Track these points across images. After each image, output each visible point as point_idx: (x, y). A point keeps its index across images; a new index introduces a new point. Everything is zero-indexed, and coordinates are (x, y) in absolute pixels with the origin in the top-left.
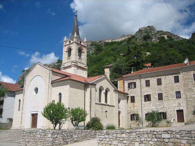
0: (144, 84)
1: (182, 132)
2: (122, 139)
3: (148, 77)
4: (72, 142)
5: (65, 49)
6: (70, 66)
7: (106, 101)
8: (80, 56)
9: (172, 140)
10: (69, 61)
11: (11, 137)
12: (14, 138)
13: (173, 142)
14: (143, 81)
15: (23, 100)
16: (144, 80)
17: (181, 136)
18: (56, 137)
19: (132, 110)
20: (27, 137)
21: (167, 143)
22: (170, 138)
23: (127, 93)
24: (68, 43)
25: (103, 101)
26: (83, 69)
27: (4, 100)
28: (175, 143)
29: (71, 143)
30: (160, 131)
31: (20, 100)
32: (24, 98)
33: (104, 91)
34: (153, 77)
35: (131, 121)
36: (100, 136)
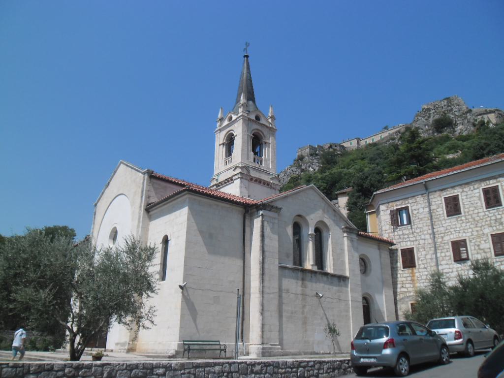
0: (442, 210)
3: (453, 187)
5: (220, 138)
10: (229, 166)
14: (438, 201)
16: (439, 199)
19: (410, 292)
23: (389, 240)
24: (226, 122)
25: (309, 263)
34: (467, 184)
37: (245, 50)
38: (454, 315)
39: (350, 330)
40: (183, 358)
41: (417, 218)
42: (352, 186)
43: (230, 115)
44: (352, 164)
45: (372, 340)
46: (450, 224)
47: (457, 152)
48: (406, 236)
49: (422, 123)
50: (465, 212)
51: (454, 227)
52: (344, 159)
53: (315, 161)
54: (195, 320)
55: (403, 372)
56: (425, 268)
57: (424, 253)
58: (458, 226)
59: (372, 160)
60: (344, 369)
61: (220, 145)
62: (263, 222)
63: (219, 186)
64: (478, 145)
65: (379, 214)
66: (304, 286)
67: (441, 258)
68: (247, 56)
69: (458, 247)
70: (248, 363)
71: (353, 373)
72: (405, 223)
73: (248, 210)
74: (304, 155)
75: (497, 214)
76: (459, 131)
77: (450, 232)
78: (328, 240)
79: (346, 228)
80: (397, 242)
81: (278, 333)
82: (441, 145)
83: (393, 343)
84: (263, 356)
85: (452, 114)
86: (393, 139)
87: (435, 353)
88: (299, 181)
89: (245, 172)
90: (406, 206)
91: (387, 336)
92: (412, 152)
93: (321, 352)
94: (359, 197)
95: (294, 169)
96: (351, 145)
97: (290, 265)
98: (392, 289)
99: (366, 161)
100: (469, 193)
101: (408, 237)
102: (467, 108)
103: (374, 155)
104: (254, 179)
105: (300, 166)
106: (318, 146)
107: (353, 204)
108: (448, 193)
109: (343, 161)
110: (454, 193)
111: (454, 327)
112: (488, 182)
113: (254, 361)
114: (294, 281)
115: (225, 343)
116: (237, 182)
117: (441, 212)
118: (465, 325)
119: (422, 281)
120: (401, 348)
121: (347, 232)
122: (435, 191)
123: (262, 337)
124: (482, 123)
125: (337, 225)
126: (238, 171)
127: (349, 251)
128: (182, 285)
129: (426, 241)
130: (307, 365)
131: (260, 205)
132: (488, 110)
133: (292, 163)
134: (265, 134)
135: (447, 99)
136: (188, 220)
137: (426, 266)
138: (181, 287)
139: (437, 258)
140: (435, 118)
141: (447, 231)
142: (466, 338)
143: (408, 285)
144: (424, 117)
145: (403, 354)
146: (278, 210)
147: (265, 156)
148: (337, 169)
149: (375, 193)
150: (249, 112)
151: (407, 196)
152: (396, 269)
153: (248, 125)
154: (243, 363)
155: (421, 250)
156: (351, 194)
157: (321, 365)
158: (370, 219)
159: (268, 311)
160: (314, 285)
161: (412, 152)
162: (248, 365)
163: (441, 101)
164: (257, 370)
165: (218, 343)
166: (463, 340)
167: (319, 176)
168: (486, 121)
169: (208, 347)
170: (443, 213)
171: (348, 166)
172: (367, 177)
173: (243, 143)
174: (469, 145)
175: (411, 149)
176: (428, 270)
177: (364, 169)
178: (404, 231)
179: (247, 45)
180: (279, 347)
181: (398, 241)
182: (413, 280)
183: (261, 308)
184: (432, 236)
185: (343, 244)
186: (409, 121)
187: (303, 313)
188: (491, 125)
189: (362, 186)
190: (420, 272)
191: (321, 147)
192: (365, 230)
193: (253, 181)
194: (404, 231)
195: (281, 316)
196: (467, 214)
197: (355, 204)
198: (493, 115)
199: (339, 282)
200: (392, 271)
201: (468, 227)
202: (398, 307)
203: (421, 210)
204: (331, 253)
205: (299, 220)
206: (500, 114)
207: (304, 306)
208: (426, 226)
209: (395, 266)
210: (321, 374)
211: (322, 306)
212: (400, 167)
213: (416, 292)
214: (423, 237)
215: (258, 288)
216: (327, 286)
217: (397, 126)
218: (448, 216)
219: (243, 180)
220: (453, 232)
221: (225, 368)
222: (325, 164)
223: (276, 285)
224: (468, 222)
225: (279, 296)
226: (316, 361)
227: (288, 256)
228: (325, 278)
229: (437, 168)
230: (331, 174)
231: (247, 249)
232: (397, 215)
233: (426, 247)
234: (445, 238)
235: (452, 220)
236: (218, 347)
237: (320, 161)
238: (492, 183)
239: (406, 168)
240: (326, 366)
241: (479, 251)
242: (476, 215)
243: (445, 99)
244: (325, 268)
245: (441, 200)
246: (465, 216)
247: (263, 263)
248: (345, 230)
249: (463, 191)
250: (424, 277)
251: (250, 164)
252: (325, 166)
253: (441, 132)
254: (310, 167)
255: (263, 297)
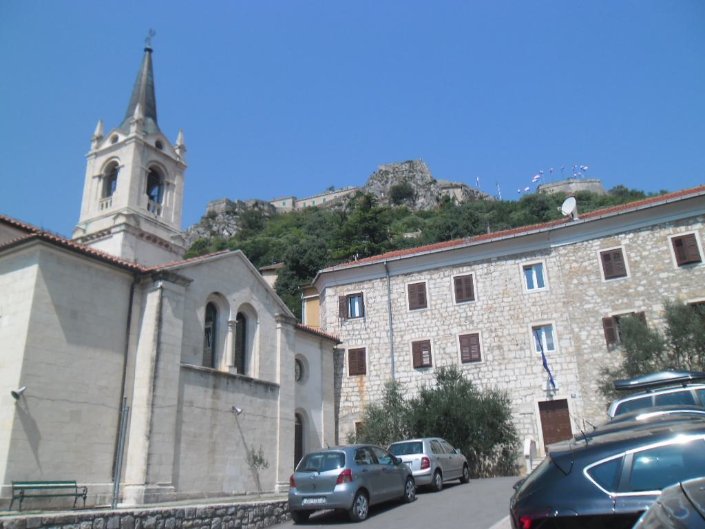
0: (403, 300)
3: (419, 272)
5: (95, 167)
14: (401, 288)
16: (402, 285)
19: (356, 407)
24: (107, 144)
25: (226, 364)
34: (437, 269)
37: (147, 40)
38: (419, 436)
39: (275, 460)
40: (10, 510)
41: (372, 309)
42: (285, 261)
43: (115, 133)
44: (284, 233)
45: (321, 473)
46: (412, 320)
47: (417, 231)
48: (357, 333)
49: (378, 189)
50: (431, 305)
51: (417, 323)
52: (273, 223)
53: (233, 222)
54: (35, 448)
55: (361, 514)
56: (377, 375)
57: (377, 356)
58: (422, 322)
59: (311, 229)
60: (277, 516)
61: (94, 177)
62: (161, 299)
63: (87, 240)
64: (445, 223)
65: (324, 300)
66: (215, 396)
67: (398, 364)
68: (150, 51)
69: (421, 351)
70: (135, 514)
71: (288, 520)
72: (357, 314)
73: (139, 279)
74: (217, 212)
75: (468, 310)
76: (420, 205)
77: (412, 329)
78: (254, 331)
79: (282, 316)
80: (344, 340)
81: (171, 467)
82: (399, 219)
83: (350, 474)
84: (146, 502)
85: (414, 183)
86: (340, 205)
87: (401, 488)
88: (208, 248)
89: (132, 223)
90: (359, 292)
91: (342, 466)
92: (366, 224)
93: (234, 492)
94: (292, 277)
95: (201, 230)
96: (284, 206)
97: (198, 365)
98: (334, 404)
99: (303, 230)
100: (439, 280)
101: (359, 334)
102: (431, 177)
103: (314, 223)
104: (146, 235)
105: (210, 227)
106: (238, 201)
107: (283, 286)
108: (413, 278)
109: (272, 226)
110: (420, 279)
111: (422, 452)
112: (461, 269)
113: (145, 510)
114: (202, 389)
115: (84, 485)
116: (118, 238)
117: (403, 304)
118: (434, 450)
119: (372, 393)
120: (358, 483)
121: (282, 322)
122: (398, 276)
123: (147, 473)
124: (447, 199)
125: (269, 311)
126: (121, 220)
127: (283, 349)
128: (17, 391)
129: (382, 339)
130: (226, 512)
131: (160, 273)
132: (454, 184)
133: (198, 221)
134: (168, 170)
135: (410, 162)
136: (37, 286)
137: (379, 373)
138: (15, 395)
139: (393, 363)
140: (393, 184)
141: (407, 328)
142: (434, 465)
143: (354, 398)
144: (380, 181)
145: (362, 491)
146: (186, 282)
147: (166, 201)
148: (263, 236)
149: (321, 271)
150: (147, 133)
151: (361, 279)
152: (340, 376)
153: (142, 153)
154: (127, 514)
155: (374, 351)
156: (281, 271)
157: (245, 512)
158: (306, 308)
159: (160, 433)
160: (230, 395)
161: (366, 224)
162: (136, 517)
163: (402, 164)
164: (150, 526)
165: (74, 485)
166: (432, 469)
167: (237, 243)
168: (451, 197)
169: (55, 492)
170: (405, 305)
171: (278, 234)
172: (306, 251)
173: (133, 179)
174: (431, 223)
175: (363, 220)
176: (382, 378)
177: (299, 241)
178: (355, 326)
179: (152, 33)
180: (172, 487)
181: (346, 339)
182: (361, 392)
183: (149, 429)
184: (389, 334)
185: (274, 339)
186: (361, 185)
187: (211, 436)
188: (457, 203)
189: (298, 262)
190: (371, 381)
191: (242, 204)
192: (301, 322)
193: (144, 238)
194: (355, 326)
195: (178, 441)
196: (433, 308)
197: (286, 285)
198: (460, 190)
199: (266, 391)
200: (335, 378)
201: (433, 325)
202: (340, 427)
203: (379, 299)
204: (257, 349)
205: (215, 300)
206: (466, 191)
207: (213, 427)
208: (383, 320)
209: (339, 373)
210: (246, 524)
211: (239, 427)
212: (349, 242)
213: (365, 408)
214: (378, 335)
215: (145, 399)
216: (248, 398)
217: (345, 188)
218: (411, 309)
219: (129, 235)
220: (416, 331)
221: (97, 524)
222: (246, 228)
223: (173, 393)
224: (434, 319)
225: (178, 411)
226: (239, 505)
227: (195, 351)
228: (246, 386)
229: (393, 248)
230: (254, 242)
231: (132, 338)
232: (347, 301)
233: (380, 348)
234: (405, 338)
235: (416, 315)
236: (73, 491)
237: (240, 223)
238: (465, 271)
239: (357, 244)
240: (252, 512)
241: (444, 355)
242: (445, 310)
243: (406, 162)
244: (248, 371)
245: (404, 288)
246: (432, 310)
247: (157, 360)
248: (280, 319)
249: (431, 279)
250: (375, 388)
251: (142, 212)
252: (246, 230)
253: (399, 204)
254: (225, 231)
255: (152, 412)
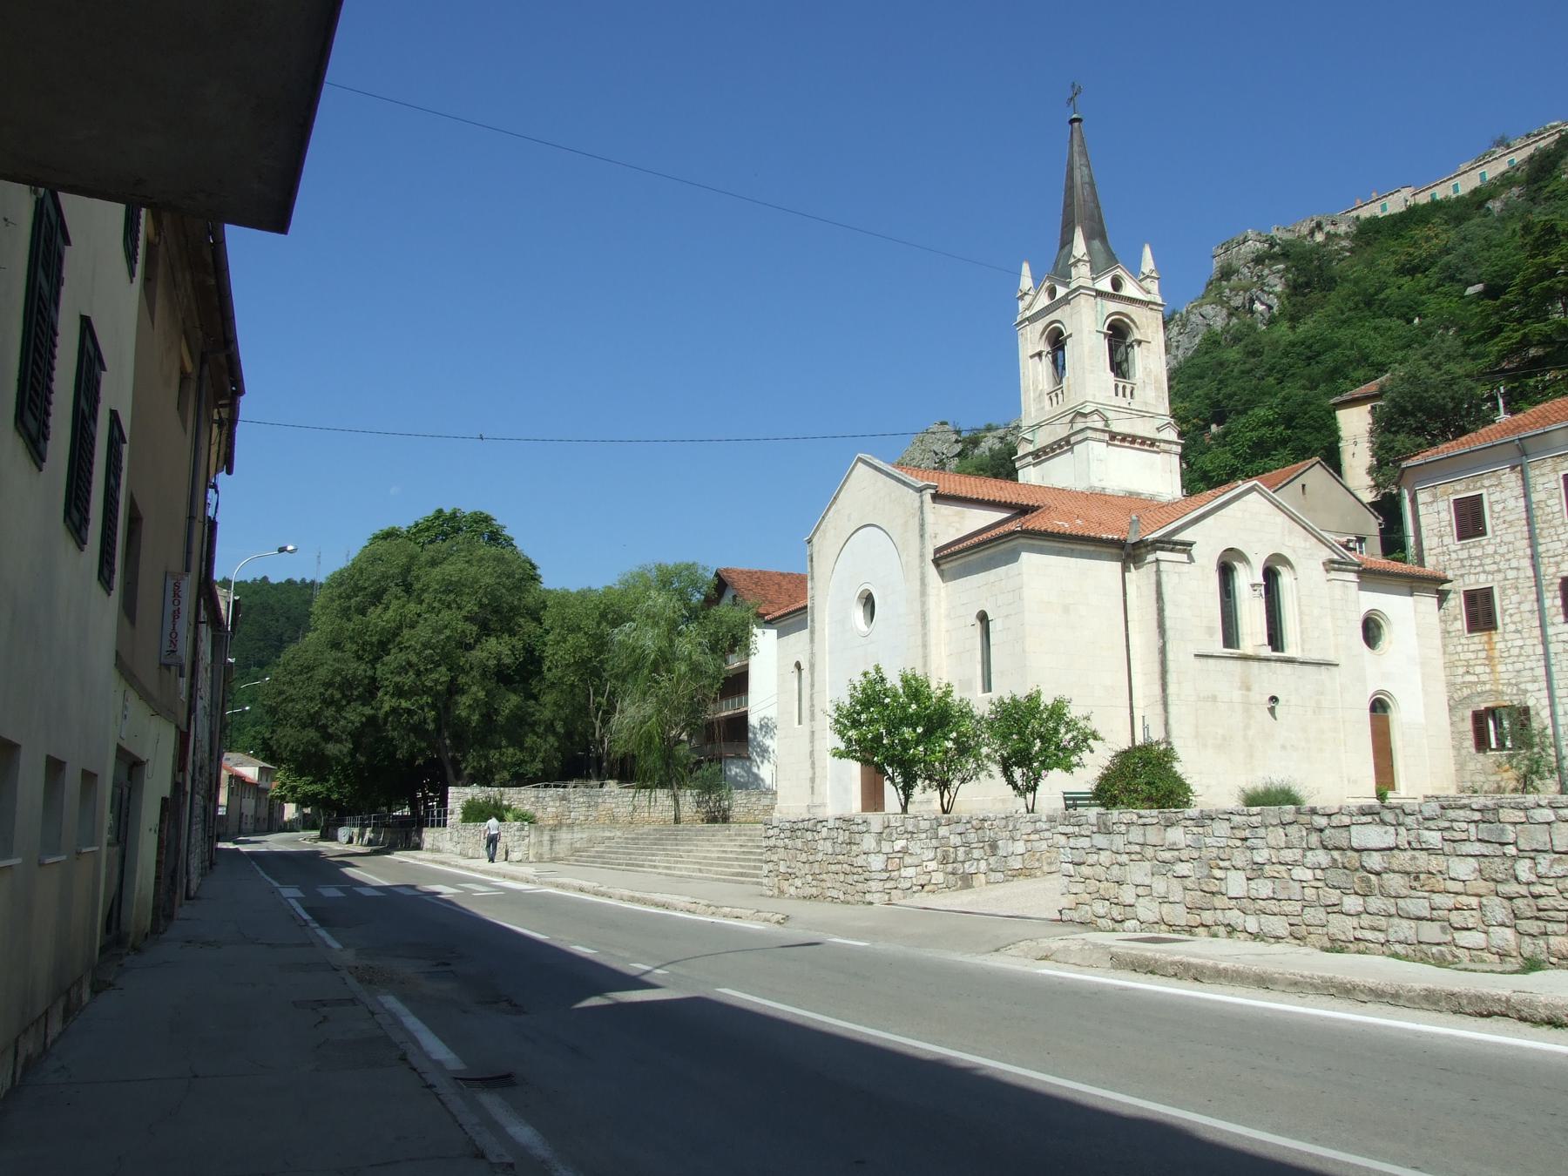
1: (1451, 814)
2: (1167, 855)
4: (993, 876)
5: (1032, 340)
6: (1067, 440)
7: (1275, 637)
8: (1119, 367)
9: (1402, 859)
11: (744, 860)
12: (755, 860)
13: (1409, 869)
15: (812, 666)
16: (1553, 477)
17: (1447, 835)
18: (905, 851)
20: (781, 853)
21: (1378, 874)
22: (1391, 849)
26: (1149, 443)
27: (747, 665)
28: (1417, 878)
29: (987, 883)
30: (1340, 812)
31: (798, 666)
32: (812, 653)
33: (1247, 579)
35: (1480, 756)
36: (1072, 842)
